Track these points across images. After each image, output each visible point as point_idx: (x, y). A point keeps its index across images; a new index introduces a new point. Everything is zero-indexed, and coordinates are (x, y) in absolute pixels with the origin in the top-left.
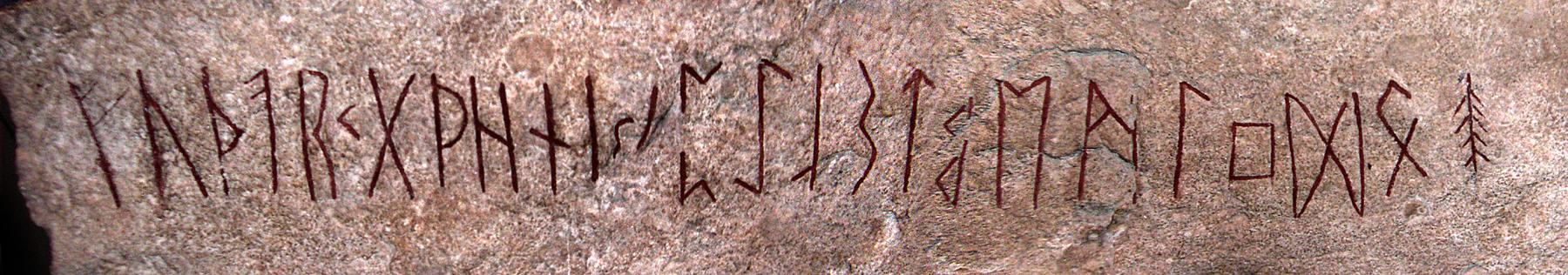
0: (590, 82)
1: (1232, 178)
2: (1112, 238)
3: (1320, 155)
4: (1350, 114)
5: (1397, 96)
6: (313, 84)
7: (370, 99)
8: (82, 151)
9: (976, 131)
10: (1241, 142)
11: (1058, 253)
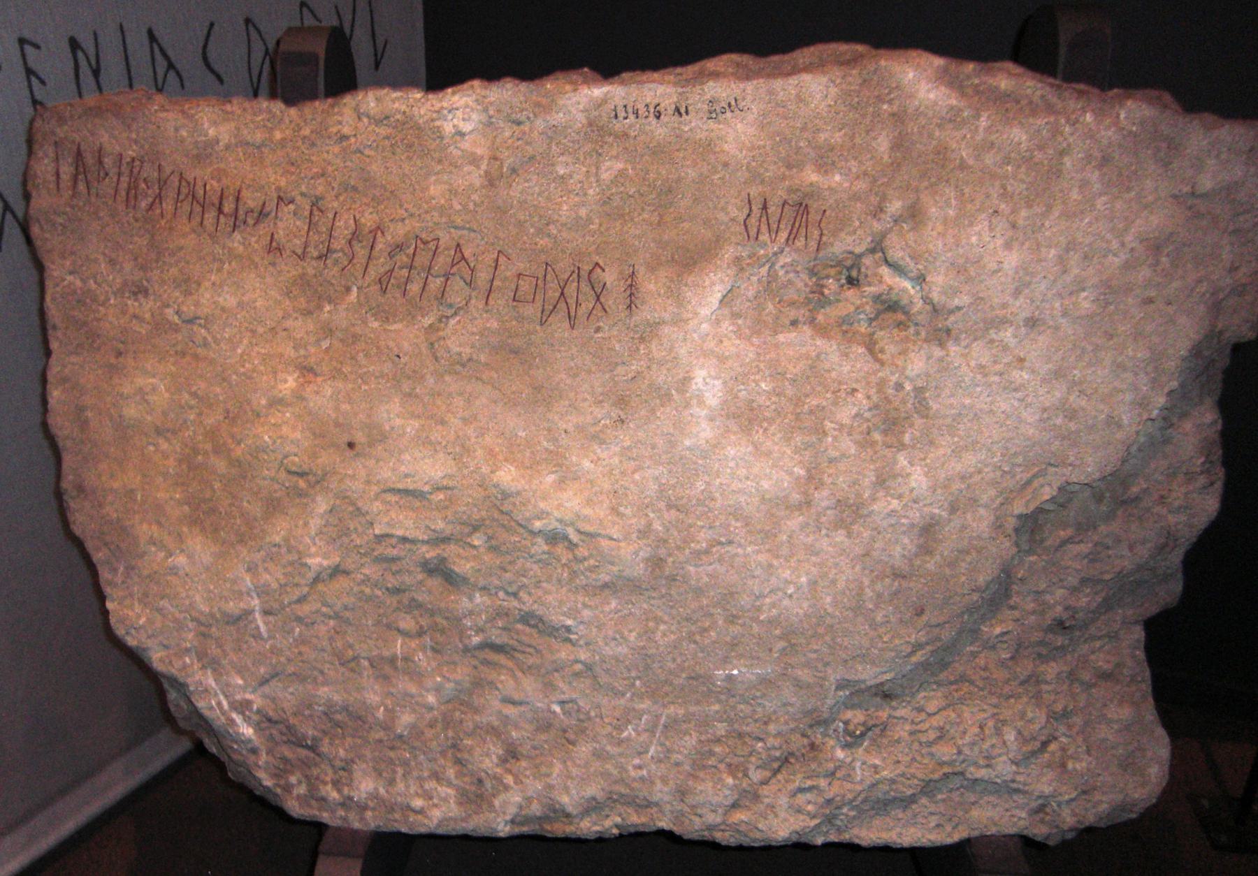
0: (239, 192)
1: (514, 300)
2: (452, 322)
3: (557, 294)
4: (575, 276)
5: (599, 270)
6: (137, 163)
7: (156, 174)
8: (51, 168)
9: (403, 258)
11: (426, 325)
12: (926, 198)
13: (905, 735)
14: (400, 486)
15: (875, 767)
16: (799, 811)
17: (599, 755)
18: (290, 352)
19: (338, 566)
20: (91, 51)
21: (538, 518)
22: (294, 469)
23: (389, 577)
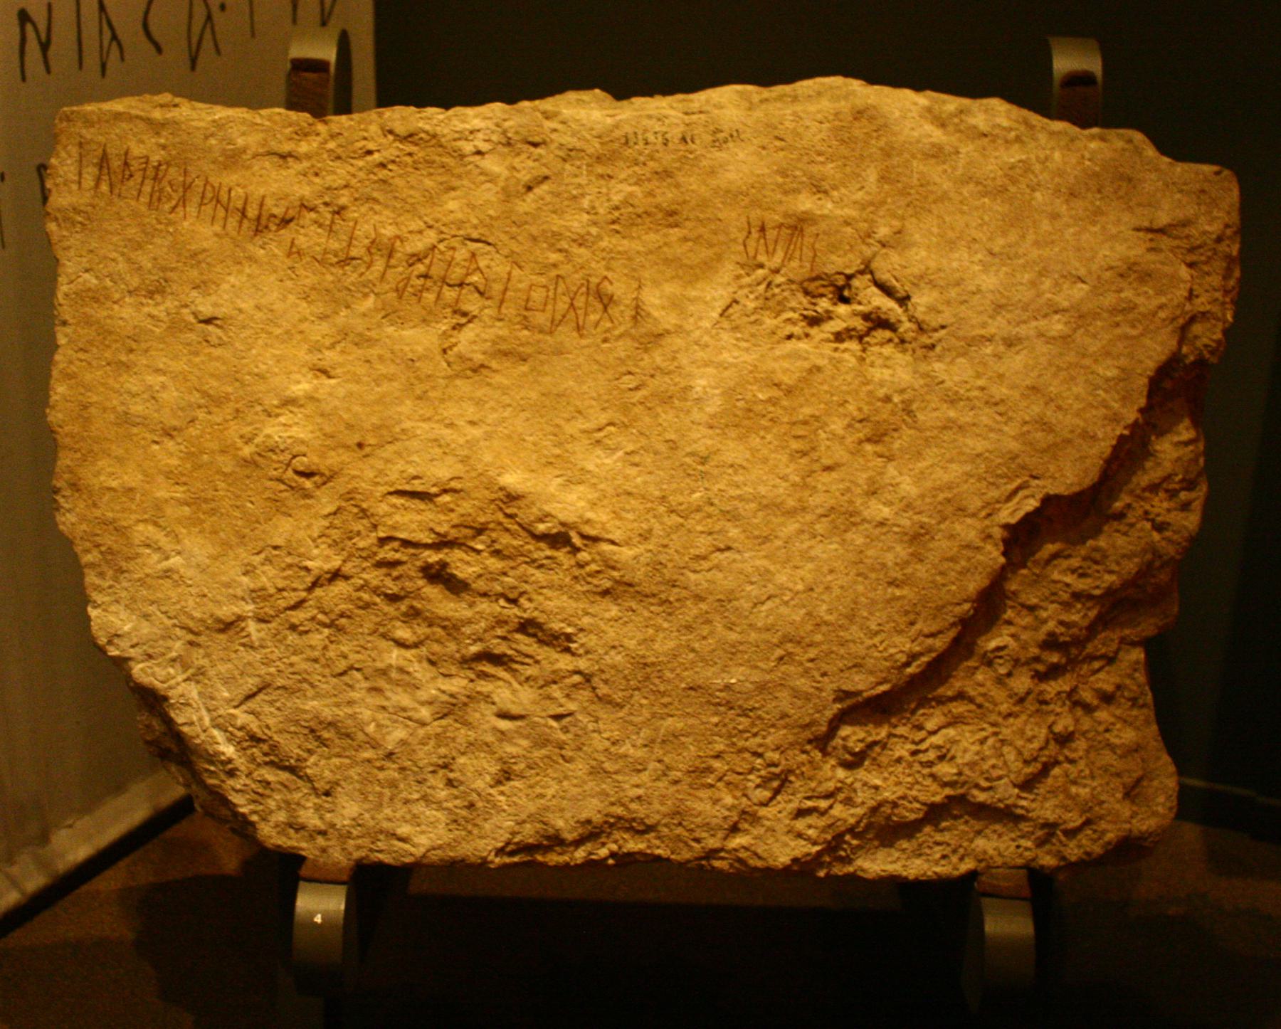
4: (584, 289)
10: (533, 294)
12: (911, 224)
13: (905, 754)
14: (408, 488)
15: (876, 788)
16: (799, 835)
17: (597, 771)
18: (303, 354)
19: (339, 570)
20: (42, 27)
21: (541, 520)
22: (301, 469)
23: (389, 582)
